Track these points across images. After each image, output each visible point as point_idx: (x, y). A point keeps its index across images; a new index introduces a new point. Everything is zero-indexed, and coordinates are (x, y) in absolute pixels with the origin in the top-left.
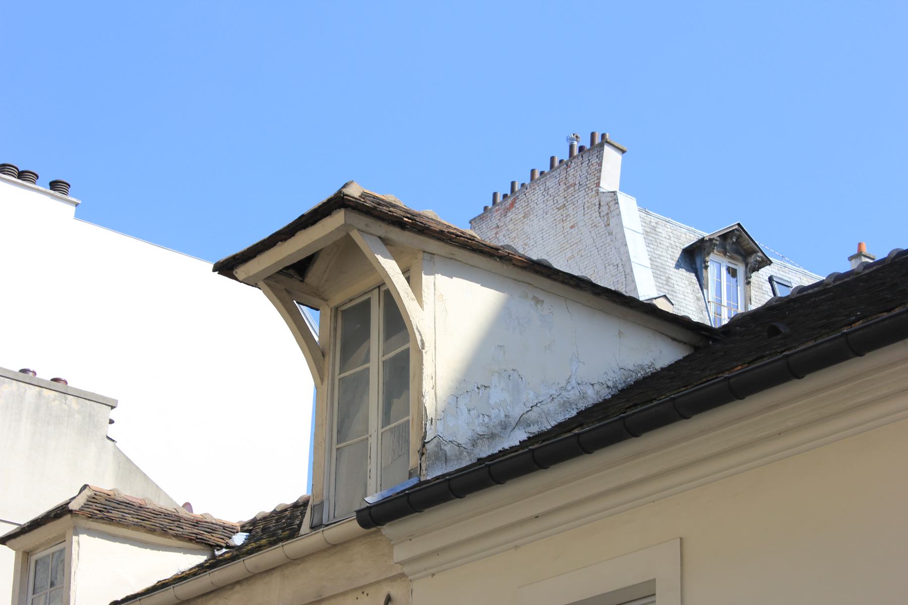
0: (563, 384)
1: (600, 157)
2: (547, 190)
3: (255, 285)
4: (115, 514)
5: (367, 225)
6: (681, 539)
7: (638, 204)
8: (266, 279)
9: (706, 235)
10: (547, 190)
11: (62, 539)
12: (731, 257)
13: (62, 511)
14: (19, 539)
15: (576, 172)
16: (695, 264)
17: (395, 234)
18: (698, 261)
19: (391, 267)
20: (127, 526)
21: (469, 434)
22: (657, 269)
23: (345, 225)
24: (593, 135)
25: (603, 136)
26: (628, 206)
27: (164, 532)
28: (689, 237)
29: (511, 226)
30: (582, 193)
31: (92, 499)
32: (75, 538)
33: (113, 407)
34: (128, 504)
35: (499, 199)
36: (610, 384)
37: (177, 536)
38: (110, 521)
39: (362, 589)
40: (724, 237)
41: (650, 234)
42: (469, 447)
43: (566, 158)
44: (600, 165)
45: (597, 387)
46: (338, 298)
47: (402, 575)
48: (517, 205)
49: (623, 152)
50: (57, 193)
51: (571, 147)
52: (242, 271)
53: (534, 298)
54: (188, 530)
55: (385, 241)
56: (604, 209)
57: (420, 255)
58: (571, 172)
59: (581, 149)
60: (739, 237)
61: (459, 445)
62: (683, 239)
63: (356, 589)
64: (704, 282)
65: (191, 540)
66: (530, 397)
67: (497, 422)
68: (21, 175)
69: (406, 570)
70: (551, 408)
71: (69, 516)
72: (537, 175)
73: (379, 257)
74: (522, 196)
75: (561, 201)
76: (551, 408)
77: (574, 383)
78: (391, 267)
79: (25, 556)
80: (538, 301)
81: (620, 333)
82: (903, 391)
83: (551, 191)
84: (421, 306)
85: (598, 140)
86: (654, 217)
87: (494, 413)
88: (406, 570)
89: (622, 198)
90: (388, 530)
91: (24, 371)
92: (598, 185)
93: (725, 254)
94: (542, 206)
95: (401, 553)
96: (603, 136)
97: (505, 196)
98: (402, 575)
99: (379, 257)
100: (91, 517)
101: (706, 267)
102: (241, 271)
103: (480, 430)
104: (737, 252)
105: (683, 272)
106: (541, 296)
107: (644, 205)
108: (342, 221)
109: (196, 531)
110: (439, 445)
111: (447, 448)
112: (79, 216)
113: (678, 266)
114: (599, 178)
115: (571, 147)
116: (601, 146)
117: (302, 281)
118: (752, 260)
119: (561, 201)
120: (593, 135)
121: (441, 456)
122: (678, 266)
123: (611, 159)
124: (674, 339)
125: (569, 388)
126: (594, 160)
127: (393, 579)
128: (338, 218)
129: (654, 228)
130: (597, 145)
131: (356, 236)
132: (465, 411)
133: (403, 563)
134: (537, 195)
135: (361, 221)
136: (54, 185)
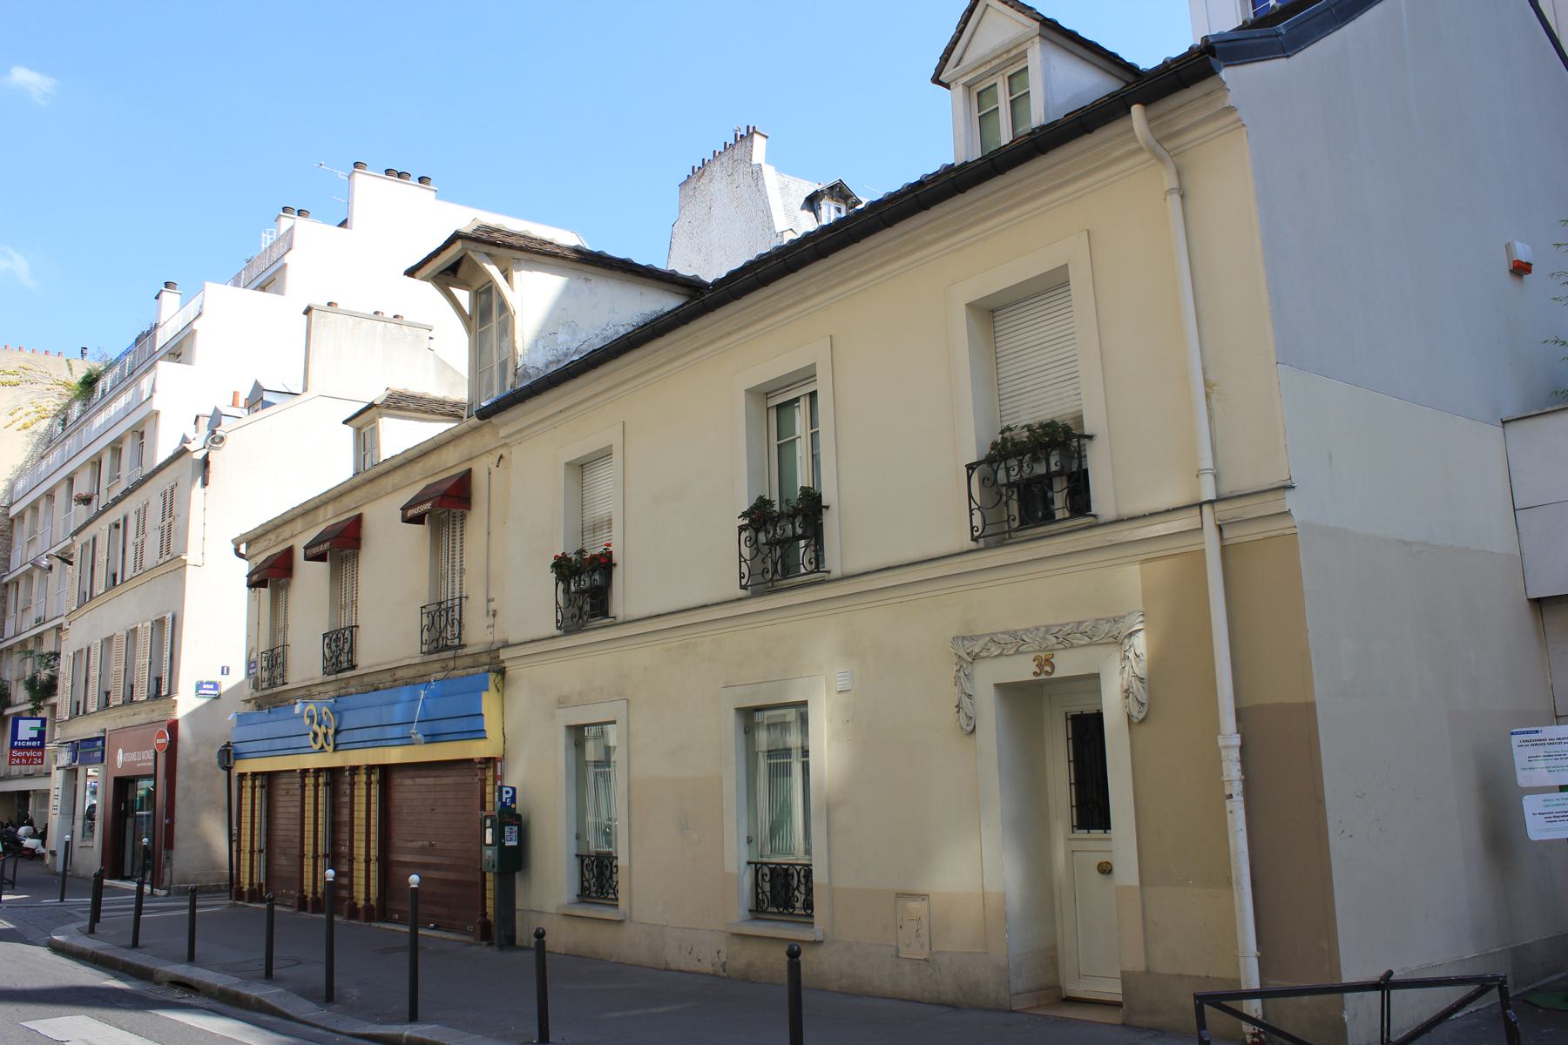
0: (604, 326)
1: (752, 141)
2: (722, 164)
3: (427, 281)
4: (403, 404)
5: (476, 247)
6: (624, 423)
7: (776, 171)
8: (434, 277)
9: (819, 188)
10: (722, 164)
11: (374, 421)
12: (836, 201)
13: (371, 406)
14: (354, 421)
15: (739, 152)
16: (813, 205)
17: (494, 250)
18: (816, 205)
19: (493, 270)
20: (410, 411)
21: (545, 361)
22: (788, 211)
23: (463, 248)
24: (748, 127)
25: (754, 128)
26: (769, 173)
27: (433, 412)
28: (809, 189)
29: (702, 188)
30: (742, 166)
31: (390, 396)
32: (380, 420)
33: (430, 330)
34: (413, 397)
35: (696, 170)
36: (635, 324)
37: (441, 414)
38: (400, 408)
39: (489, 452)
40: (832, 188)
41: (784, 189)
42: (544, 369)
43: (733, 143)
44: (752, 147)
45: (626, 326)
46: (476, 286)
47: (506, 444)
48: (705, 174)
49: (767, 137)
50: (423, 185)
51: (736, 135)
52: (418, 274)
53: (585, 278)
54: (449, 408)
55: (488, 255)
56: (755, 175)
57: (512, 260)
58: (736, 152)
59: (741, 136)
60: (841, 188)
61: (538, 368)
62: (806, 191)
63: (487, 452)
64: (819, 218)
65: (450, 416)
66: (582, 336)
67: (561, 352)
68: (400, 175)
69: (507, 441)
70: (596, 342)
71: (375, 408)
72: (717, 154)
73: (485, 265)
74: (708, 168)
75: (730, 171)
76: (596, 342)
77: (611, 326)
78: (493, 270)
79: (358, 430)
80: (587, 280)
81: (641, 294)
82: (729, 334)
83: (725, 164)
84: (512, 289)
85: (751, 131)
86: (787, 178)
87: (560, 348)
88: (507, 441)
89: (765, 167)
90: (495, 420)
91: (376, 313)
92: (751, 160)
93: (832, 199)
94: (720, 174)
95: (502, 433)
96: (754, 128)
97: (699, 168)
98: (506, 444)
99: (485, 265)
100: (388, 407)
101: (820, 208)
102: (417, 274)
103: (550, 359)
104: (841, 197)
105: (805, 212)
106: (589, 277)
107: (781, 170)
108: (461, 247)
109: (453, 409)
110: (525, 370)
111: (530, 371)
112: (438, 198)
113: (802, 209)
114: (751, 155)
115: (736, 135)
116: (752, 134)
117: (455, 277)
118: (850, 201)
119: (730, 171)
120: (748, 127)
121: (526, 375)
122: (802, 209)
123: (758, 141)
124: (677, 293)
125: (608, 328)
126: (749, 144)
127: (503, 446)
128: (458, 245)
129: (787, 186)
130: (750, 133)
131: (470, 253)
132: (542, 349)
133: (505, 437)
134: (716, 168)
135: (472, 245)
136: (421, 180)
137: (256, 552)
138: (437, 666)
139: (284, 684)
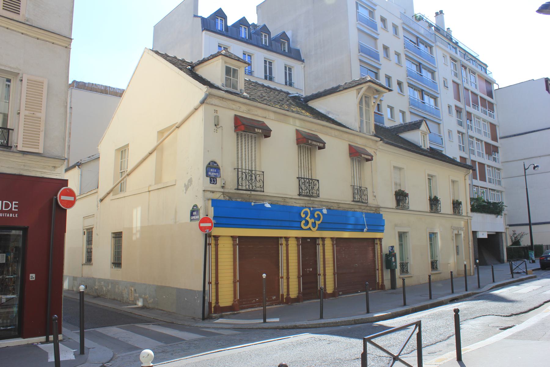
137: (220, 105)
138: (357, 207)
139: (263, 191)
